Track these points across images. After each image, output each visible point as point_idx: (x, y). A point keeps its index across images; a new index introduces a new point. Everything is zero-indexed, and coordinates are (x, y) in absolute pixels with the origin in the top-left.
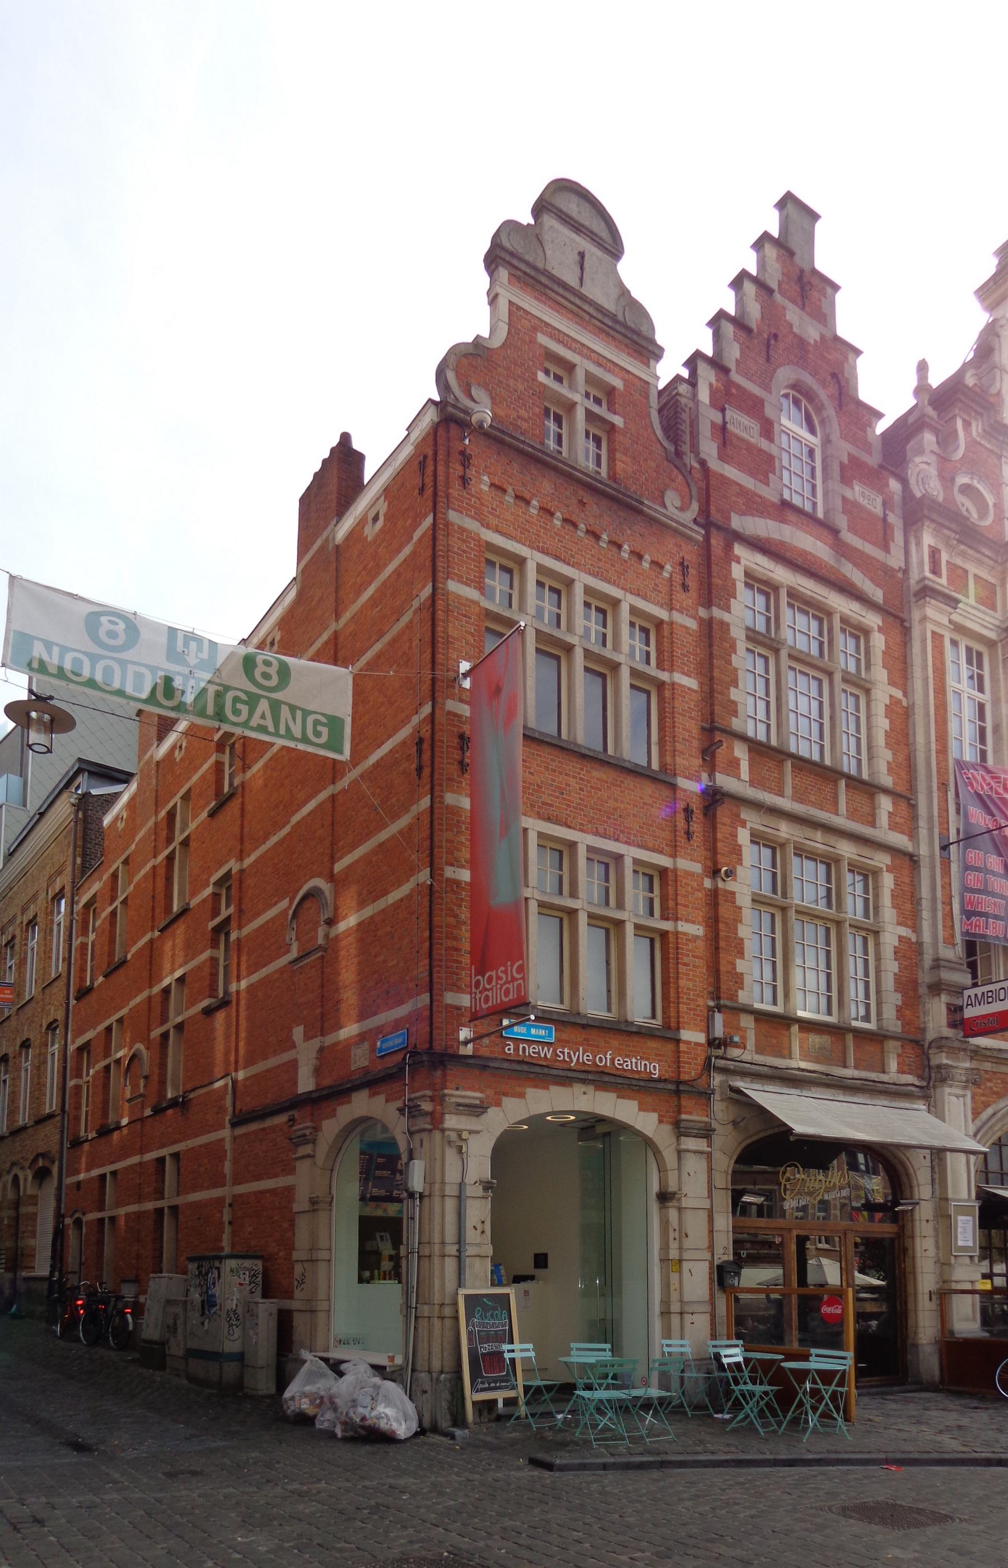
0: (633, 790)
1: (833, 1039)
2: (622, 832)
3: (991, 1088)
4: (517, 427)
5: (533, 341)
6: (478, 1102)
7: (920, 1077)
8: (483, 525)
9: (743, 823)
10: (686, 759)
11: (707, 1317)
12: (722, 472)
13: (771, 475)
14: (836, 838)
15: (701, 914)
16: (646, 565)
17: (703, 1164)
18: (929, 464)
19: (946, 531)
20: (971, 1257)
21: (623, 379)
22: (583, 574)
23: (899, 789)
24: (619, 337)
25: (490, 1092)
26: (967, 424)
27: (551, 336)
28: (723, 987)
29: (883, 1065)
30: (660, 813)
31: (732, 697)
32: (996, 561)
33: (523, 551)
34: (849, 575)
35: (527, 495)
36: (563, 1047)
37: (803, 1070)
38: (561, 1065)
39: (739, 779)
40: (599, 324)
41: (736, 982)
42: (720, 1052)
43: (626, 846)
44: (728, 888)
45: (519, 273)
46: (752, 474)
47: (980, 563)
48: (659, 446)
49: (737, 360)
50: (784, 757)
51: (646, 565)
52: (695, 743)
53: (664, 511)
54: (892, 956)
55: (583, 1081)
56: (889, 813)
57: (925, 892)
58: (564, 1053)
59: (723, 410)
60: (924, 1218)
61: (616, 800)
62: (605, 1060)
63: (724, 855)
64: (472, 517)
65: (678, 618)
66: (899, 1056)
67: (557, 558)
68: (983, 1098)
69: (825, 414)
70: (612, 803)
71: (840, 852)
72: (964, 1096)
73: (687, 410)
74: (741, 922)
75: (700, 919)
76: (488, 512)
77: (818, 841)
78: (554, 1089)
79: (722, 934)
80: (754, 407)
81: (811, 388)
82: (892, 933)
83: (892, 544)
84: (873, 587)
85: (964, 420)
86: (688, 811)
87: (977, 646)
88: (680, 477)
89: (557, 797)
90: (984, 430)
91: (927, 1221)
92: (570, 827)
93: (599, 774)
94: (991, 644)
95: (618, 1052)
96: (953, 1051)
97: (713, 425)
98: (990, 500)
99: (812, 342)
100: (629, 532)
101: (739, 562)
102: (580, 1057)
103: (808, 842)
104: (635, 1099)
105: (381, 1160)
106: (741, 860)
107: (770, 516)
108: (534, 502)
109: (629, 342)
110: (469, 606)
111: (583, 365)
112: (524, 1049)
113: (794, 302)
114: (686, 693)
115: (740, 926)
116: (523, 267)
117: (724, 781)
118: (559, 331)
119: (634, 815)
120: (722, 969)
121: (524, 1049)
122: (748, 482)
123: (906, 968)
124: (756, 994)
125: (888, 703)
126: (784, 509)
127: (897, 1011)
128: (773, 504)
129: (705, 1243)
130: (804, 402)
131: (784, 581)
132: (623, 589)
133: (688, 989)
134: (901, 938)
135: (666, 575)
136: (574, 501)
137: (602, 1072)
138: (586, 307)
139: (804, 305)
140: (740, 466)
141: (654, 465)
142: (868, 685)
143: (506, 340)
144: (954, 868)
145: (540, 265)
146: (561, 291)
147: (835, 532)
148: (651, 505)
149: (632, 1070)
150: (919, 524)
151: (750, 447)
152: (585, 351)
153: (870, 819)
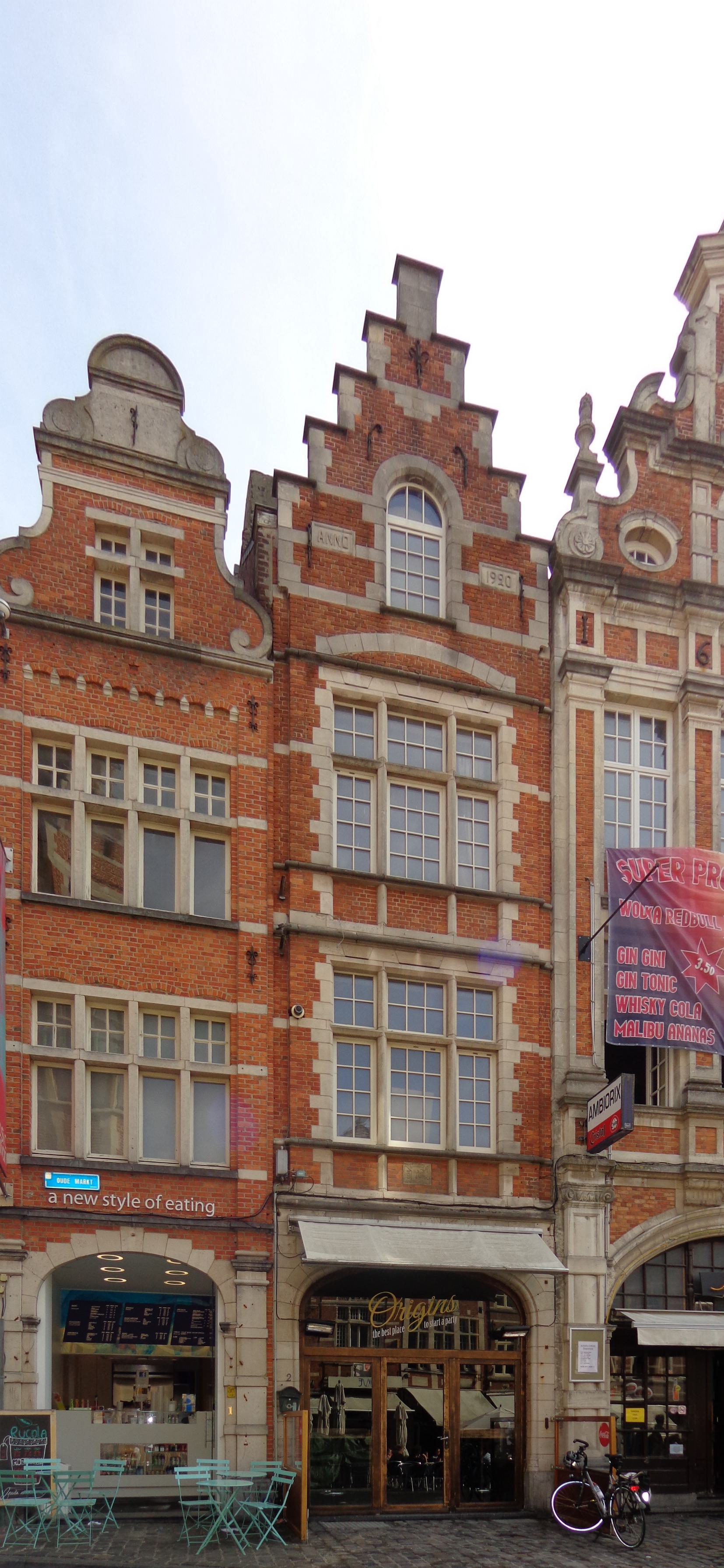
0: (191, 943)
1: (435, 1166)
2: (178, 984)
3: (640, 1205)
4: (61, 608)
5: (81, 516)
6: (20, 1248)
7: (542, 1197)
8: (25, 713)
9: (322, 958)
10: (251, 902)
11: (264, 1439)
12: (304, 595)
13: (368, 585)
14: (440, 958)
15: (266, 1054)
16: (210, 714)
17: (262, 1296)
18: (585, 518)
19: (597, 590)
20: (597, 1384)
21: (185, 528)
22: (137, 739)
23: (529, 895)
24: (177, 484)
25: (33, 1239)
26: (642, 456)
27: (101, 507)
28: (294, 1124)
29: (498, 1189)
30: (220, 961)
31: (312, 830)
32: (673, 608)
33: (70, 729)
34: (468, 671)
35: (72, 673)
36: (111, 1193)
37: (389, 1200)
38: (109, 1211)
39: (318, 912)
40: (153, 477)
41: (309, 1118)
42: (286, 1188)
43: (183, 998)
44: (301, 1026)
45: (62, 452)
46: (344, 589)
47: (655, 615)
48: (226, 586)
49: (328, 469)
50: (377, 882)
51: (210, 714)
52: (262, 884)
53: (230, 654)
54: (512, 1075)
55: (130, 1224)
56: (514, 921)
57: (558, 1001)
58: (110, 1200)
59: (308, 529)
60: (543, 1343)
61: (171, 955)
62: (154, 1203)
63: (298, 993)
64: (12, 708)
65: (245, 760)
66: (515, 1178)
67: (108, 728)
68: (628, 1217)
69: (445, 497)
70: (166, 959)
71: (445, 972)
72: (596, 1216)
73: (270, 540)
74: (317, 1058)
75: (264, 1060)
76: (34, 699)
77: (417, 964)
78: (99, 1232)
79: (294, 1072)
80: (348, 515)
81: (426, 473)
82: (513, 1048)
83: (531, 622)
84: (502, 676)
85: (638, 452)
86: (252, 955)
87: (655, 714)
88: (251, 613)
89: (107, 961)
90: (662, 455)
91: (547, 1347)
92: (120, 988)
93: (152, 932)
94: (671, 707)
95: (173, 1195)
96: (579, 1170)
97: (296, 547)
98: (672, 538)
99: (429, 420)
100: (187, 684)
101: (324, 687)
102: (130, 1201)
103: (403, 967)
104: (187, 1238)
105: (129, 1308)
106: (319, 995)
107: (365, 629)
108: (80, 679)
109: (189, 487)
110: (10, 795)
111: (137, 525)
112: (68, 1198)
113: (406, 381)
114: (253, 835)
115: (315, 1062)
116: (64, 444)
117: (299, 918)
118: (110, 498)
119: (192, 967)
120: (293, 1106)
121: (68, 1198)
122: (337, 598)
123: (529, 1086)
124: (329, 1127)
125: (518, 801)
126: (385, 617)
127: (515, 1132)
128: (371, 616)
129: (263, 1370)
130: (424, 491)
131: (381, 695)
132: (183, 744)
133: (248, 1129)
134: (523, 1055)
135: (233, 719)
136: (125, 666)
137: (151, 1215)
138: (136, 464)
139: (419, 382)
140: (330, 584)
141: (220, 608)
142: (493, 788)
143: (51, 525)
144: (596, 970)
145: (88, 438)
146: (107, 456)
147: (449, 626)
148: (209, 650)
149: (184, 1211)
150: (564, 590)
151: (342, 560)
152: (140, 511)
153: (492, 931)
